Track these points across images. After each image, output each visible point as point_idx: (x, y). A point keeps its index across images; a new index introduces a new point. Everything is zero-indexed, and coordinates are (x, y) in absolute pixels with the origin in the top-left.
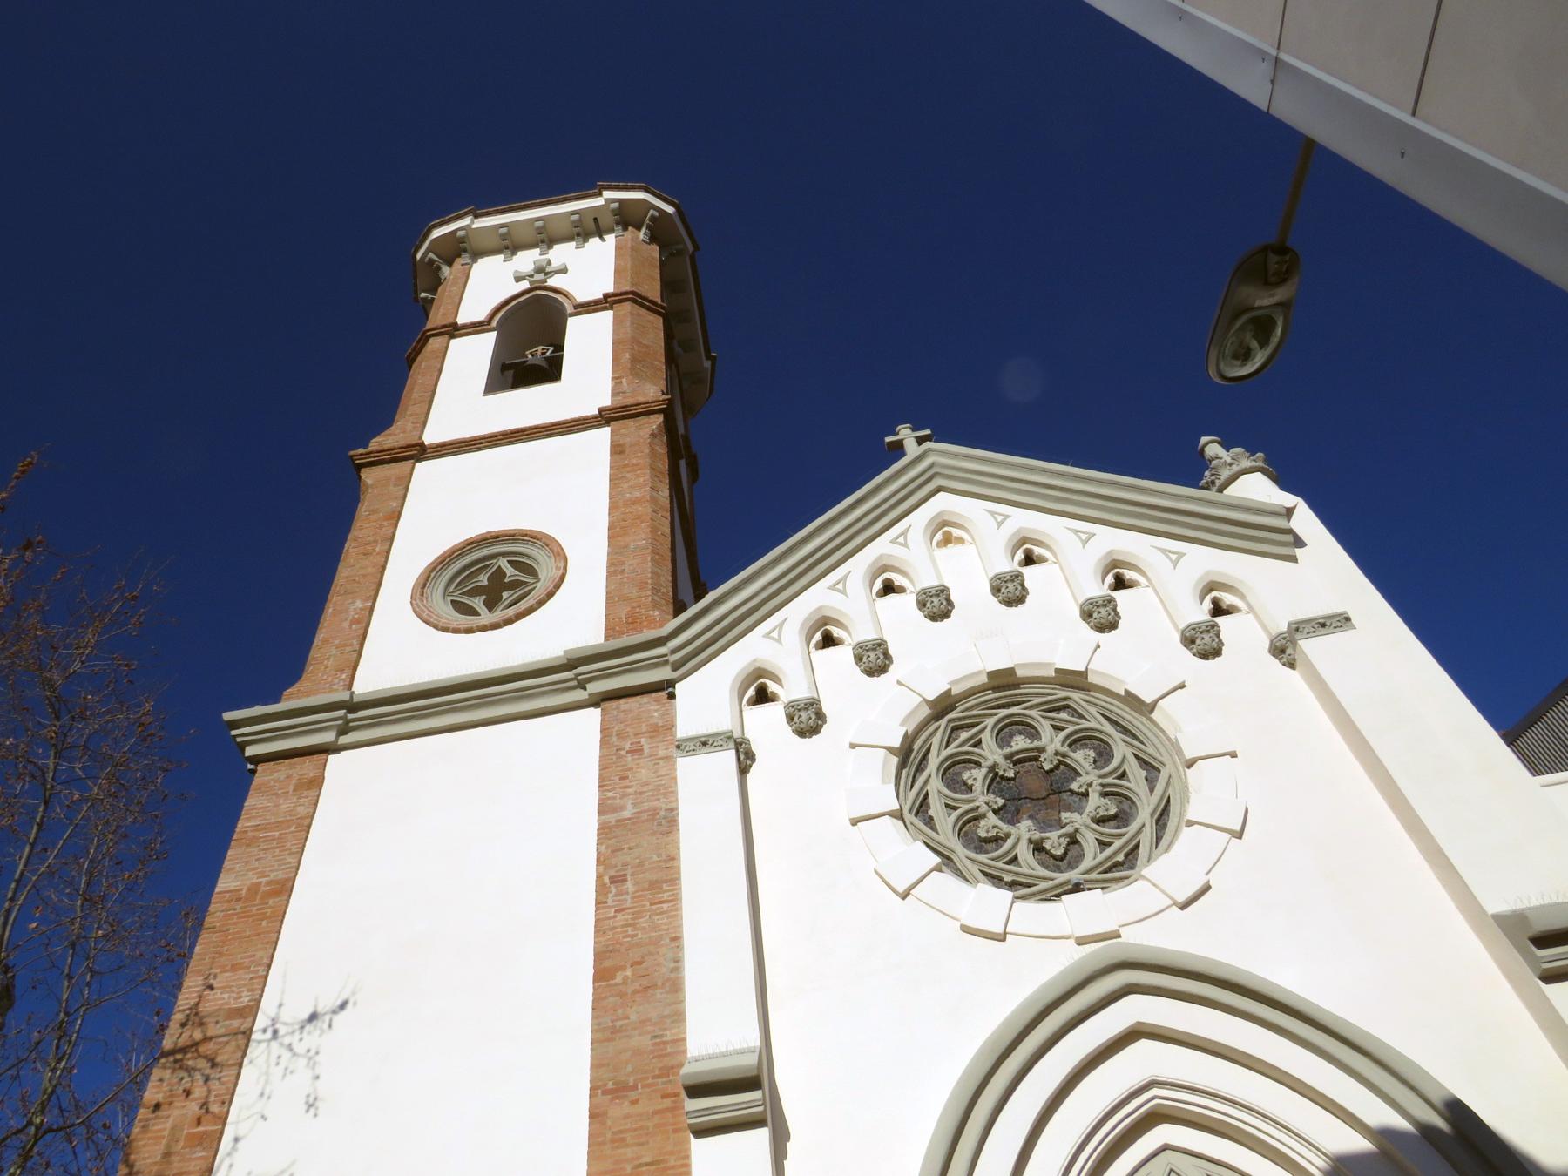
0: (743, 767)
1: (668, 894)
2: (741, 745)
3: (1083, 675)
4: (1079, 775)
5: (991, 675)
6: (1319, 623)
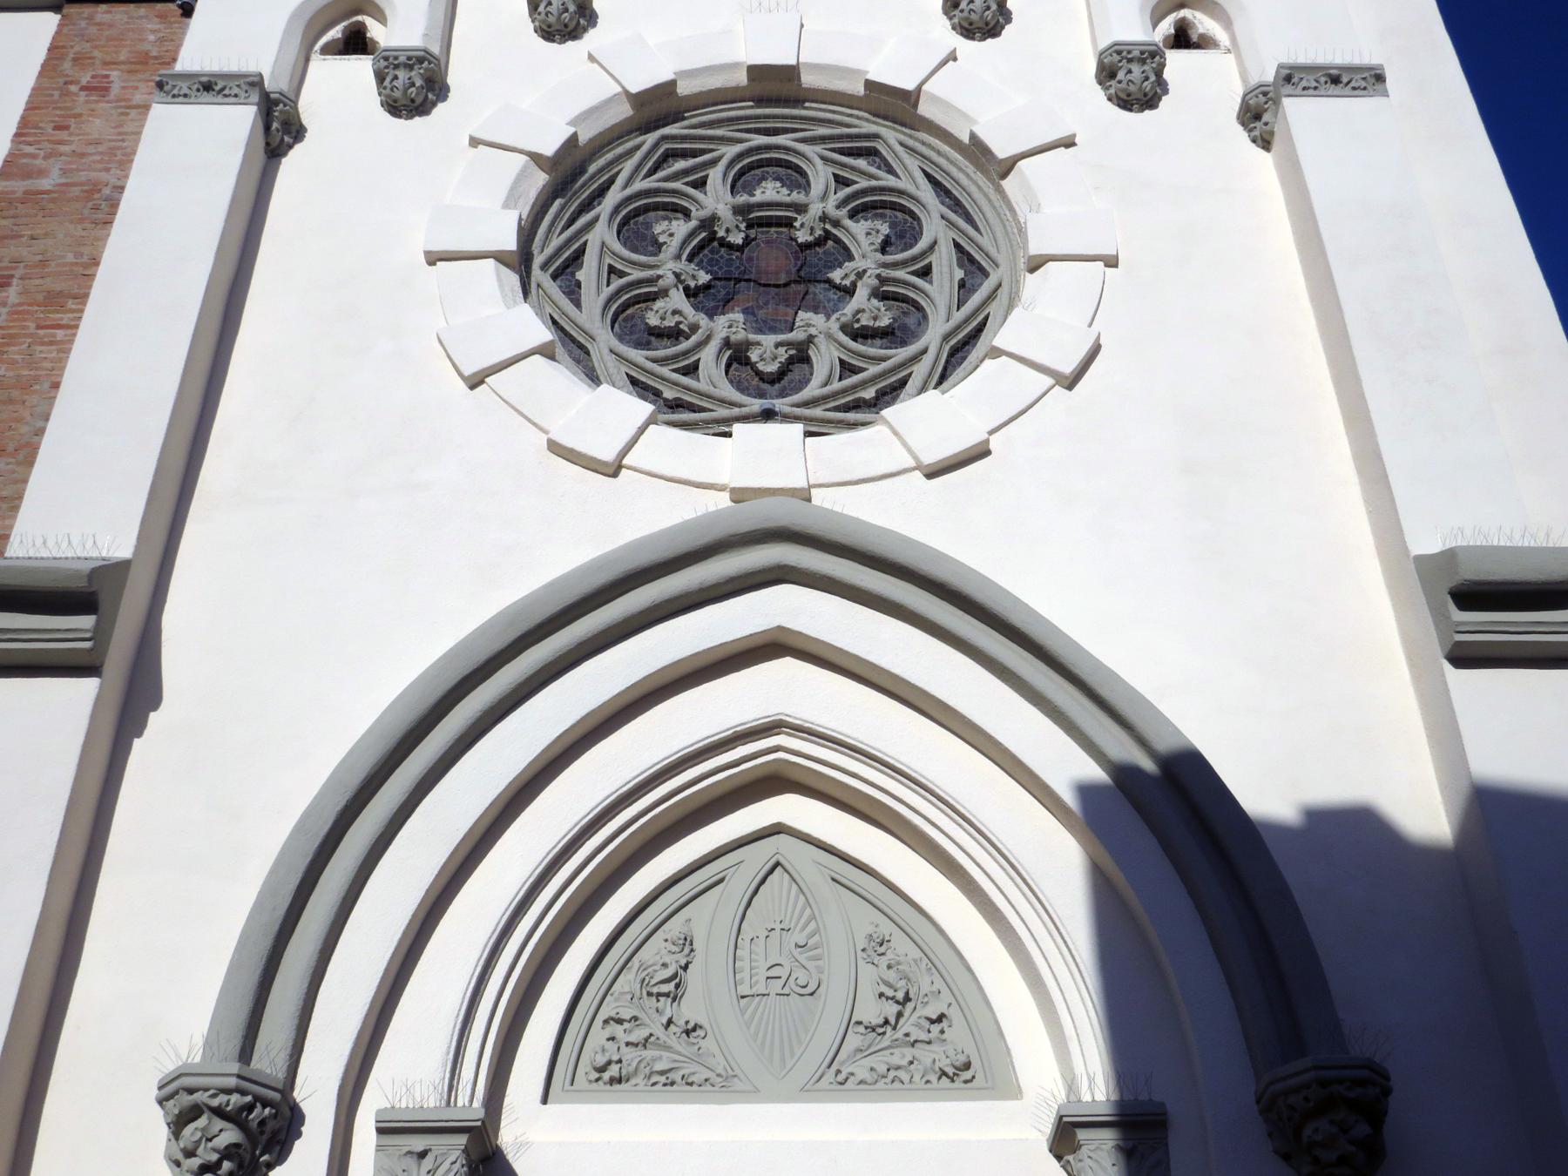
0: (275, 142)
1: (71, 315)
2: (277, 105)
3: (909, 98)
4: (850, 258)
5: (756, 72)
6: (1330, 76)
